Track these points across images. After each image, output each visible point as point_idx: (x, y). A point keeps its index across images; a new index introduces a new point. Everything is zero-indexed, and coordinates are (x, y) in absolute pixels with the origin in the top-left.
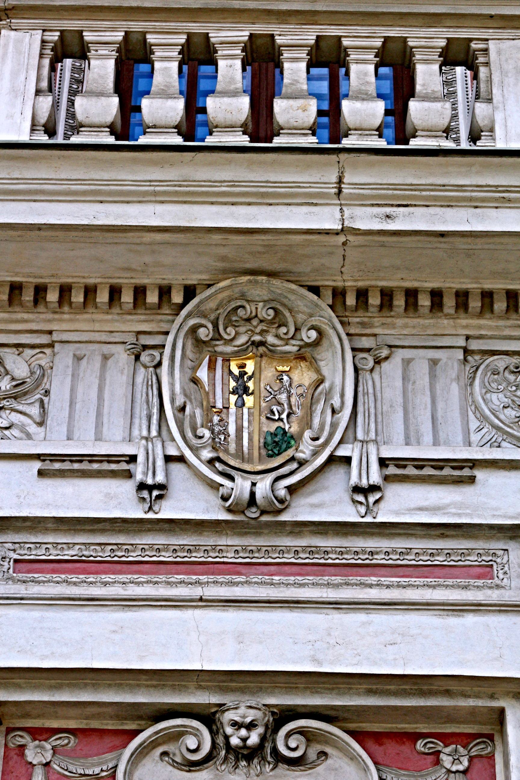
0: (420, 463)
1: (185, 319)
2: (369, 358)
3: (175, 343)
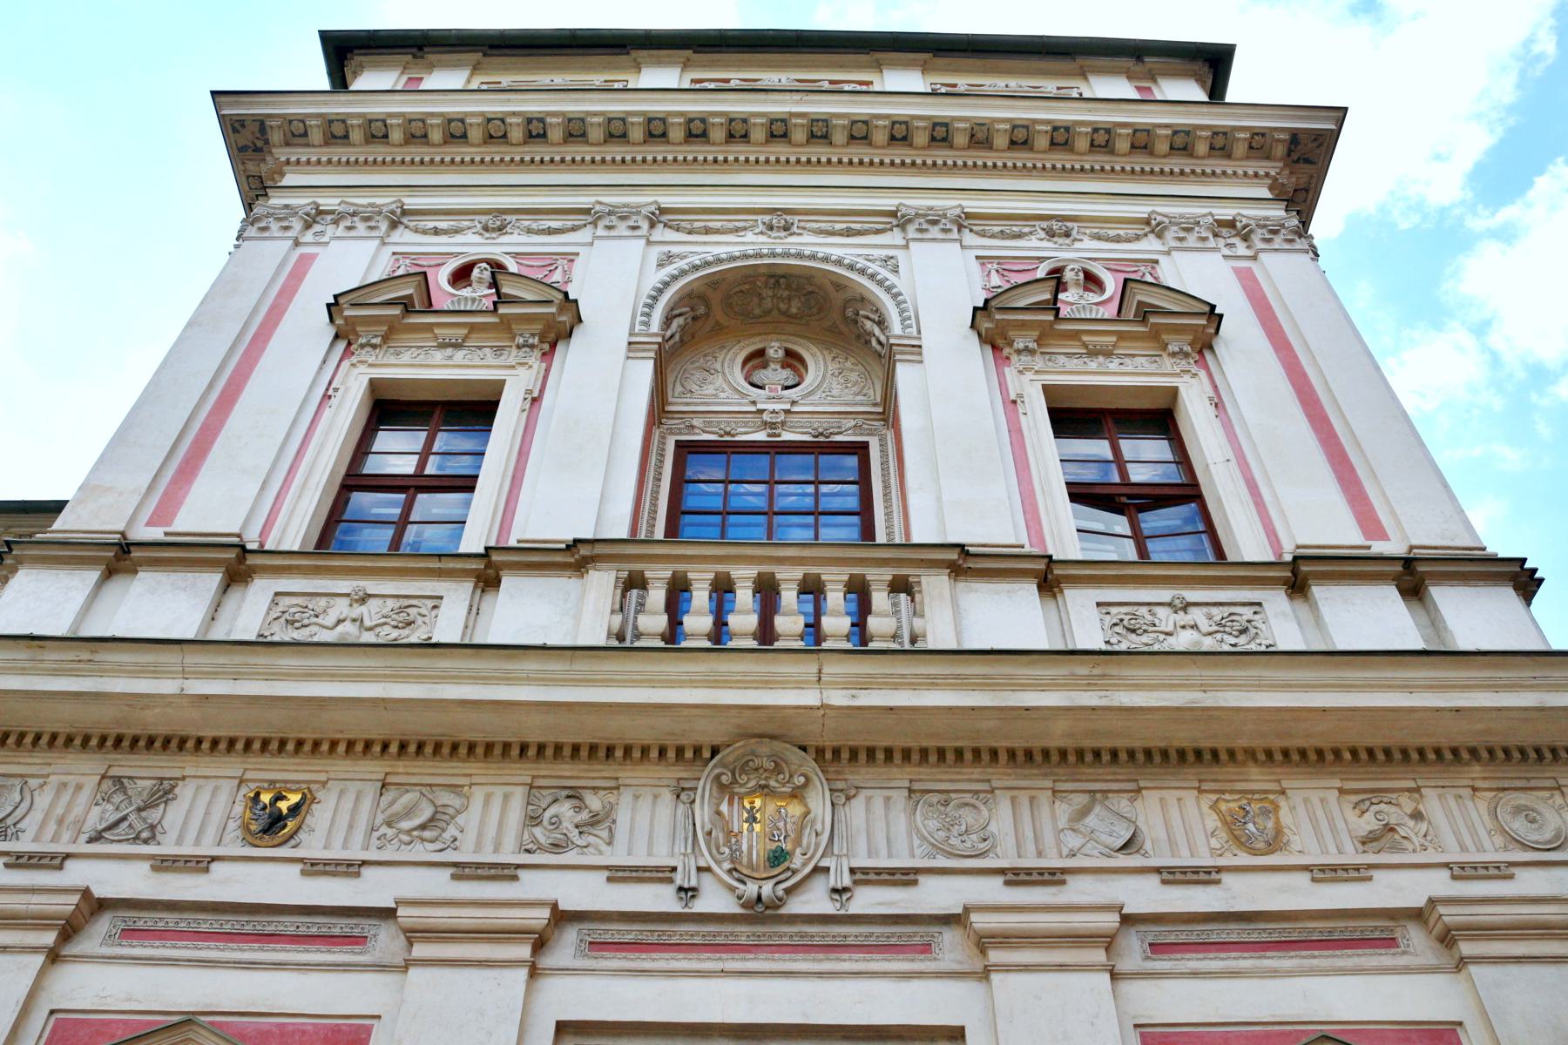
0: (878, 871)
1: (712, 769)
2: (842, 796)
3: (705, 787)
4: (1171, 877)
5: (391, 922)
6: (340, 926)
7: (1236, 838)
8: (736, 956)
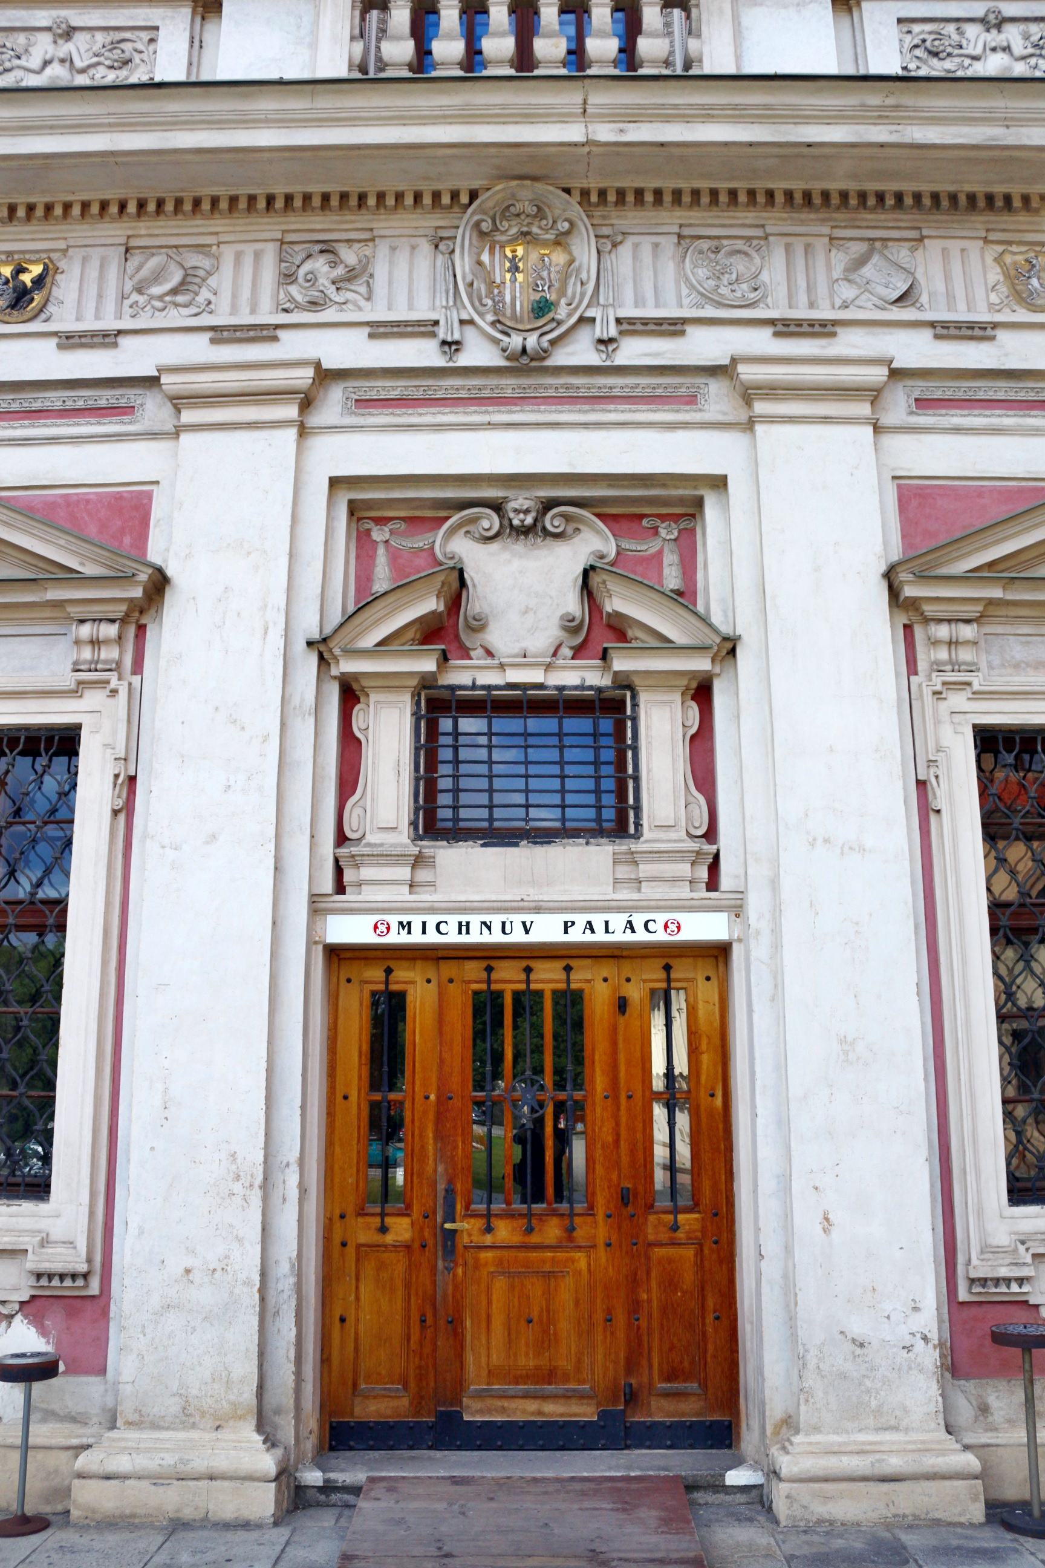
0: (645, 322)
1: (471, 215)
3: (464, 236)
4: (945, 332)
5: (156, 390)
6: (106, 397)
7: (1018, 293)
8: (503, 408)
